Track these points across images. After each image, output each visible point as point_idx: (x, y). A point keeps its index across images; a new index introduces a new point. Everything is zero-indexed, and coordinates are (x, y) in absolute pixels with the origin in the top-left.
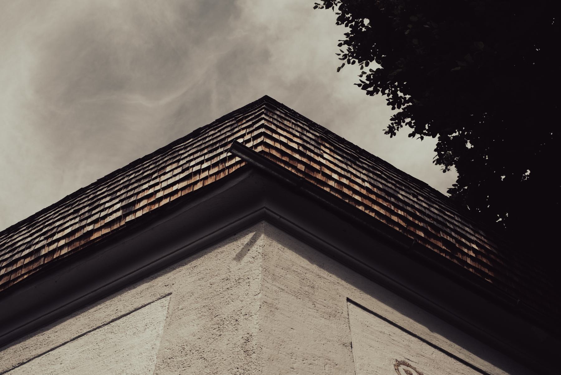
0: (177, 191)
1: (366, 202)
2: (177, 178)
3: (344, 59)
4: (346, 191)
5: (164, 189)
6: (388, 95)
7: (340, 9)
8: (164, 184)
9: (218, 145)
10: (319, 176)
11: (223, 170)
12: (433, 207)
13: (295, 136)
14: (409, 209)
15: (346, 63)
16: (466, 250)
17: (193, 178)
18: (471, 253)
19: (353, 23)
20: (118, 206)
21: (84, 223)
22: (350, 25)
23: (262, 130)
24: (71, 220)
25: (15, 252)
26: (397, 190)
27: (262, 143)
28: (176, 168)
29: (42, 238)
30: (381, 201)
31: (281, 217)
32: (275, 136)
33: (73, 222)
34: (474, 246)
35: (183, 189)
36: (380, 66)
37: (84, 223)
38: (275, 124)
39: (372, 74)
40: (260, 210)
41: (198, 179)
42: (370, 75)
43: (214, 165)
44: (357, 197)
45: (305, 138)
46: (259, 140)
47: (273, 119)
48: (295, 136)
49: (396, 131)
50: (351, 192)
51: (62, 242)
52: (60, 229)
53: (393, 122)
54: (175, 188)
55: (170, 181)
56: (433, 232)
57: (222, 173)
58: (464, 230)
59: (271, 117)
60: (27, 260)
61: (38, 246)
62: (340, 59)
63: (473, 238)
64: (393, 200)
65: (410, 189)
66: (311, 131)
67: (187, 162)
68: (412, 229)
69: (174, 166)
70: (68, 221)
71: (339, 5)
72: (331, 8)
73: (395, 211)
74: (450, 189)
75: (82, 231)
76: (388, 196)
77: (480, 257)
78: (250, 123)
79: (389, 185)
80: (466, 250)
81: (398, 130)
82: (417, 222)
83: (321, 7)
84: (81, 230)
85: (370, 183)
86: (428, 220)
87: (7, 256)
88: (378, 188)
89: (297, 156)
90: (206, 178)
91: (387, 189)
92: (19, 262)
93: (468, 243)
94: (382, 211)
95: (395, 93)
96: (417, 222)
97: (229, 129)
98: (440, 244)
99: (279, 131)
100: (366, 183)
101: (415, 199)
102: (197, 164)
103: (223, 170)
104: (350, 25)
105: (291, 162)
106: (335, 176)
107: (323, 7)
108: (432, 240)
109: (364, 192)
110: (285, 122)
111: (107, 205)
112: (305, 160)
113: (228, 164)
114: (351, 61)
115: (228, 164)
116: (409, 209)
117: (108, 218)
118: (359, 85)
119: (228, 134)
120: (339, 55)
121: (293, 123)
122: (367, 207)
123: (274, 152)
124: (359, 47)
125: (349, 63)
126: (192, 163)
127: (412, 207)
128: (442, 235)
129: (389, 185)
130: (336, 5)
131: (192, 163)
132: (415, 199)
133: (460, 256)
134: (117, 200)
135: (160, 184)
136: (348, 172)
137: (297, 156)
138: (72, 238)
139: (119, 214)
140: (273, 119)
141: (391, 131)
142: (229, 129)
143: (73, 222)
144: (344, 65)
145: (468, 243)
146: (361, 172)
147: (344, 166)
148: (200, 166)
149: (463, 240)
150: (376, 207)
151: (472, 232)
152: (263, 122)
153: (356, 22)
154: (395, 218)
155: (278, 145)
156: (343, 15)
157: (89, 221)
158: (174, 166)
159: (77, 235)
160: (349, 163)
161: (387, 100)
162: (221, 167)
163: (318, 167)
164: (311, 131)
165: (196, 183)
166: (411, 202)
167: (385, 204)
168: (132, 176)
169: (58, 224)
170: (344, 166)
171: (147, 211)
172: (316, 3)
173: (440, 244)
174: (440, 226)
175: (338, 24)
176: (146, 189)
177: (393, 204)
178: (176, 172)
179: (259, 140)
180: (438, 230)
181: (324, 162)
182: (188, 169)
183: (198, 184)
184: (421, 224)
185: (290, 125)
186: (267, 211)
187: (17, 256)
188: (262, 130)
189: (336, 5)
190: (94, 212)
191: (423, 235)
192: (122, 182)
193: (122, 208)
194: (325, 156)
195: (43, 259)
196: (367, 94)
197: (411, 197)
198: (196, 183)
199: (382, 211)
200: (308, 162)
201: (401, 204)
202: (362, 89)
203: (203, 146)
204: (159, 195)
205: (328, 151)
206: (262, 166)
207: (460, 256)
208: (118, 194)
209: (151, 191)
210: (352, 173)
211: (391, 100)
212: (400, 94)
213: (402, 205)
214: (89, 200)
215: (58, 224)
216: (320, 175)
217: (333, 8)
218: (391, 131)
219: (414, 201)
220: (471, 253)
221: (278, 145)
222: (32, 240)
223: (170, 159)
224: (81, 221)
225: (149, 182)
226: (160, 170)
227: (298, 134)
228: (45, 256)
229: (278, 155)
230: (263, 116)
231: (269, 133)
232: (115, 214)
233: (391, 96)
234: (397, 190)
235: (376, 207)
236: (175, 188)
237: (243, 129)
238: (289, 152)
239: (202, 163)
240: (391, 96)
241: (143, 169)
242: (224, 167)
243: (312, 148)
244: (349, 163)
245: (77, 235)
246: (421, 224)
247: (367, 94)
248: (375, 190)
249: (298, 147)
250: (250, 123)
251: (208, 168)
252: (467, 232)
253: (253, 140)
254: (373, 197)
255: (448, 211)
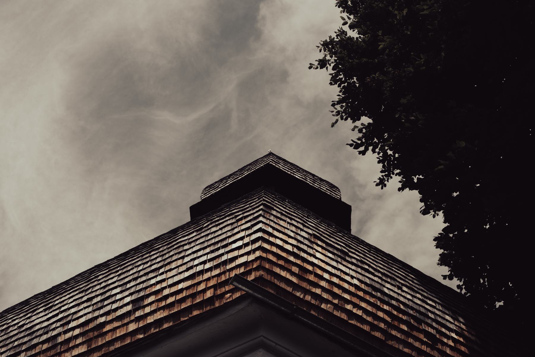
0: (181, 291)
1: (355, 300)
2: (182, 277)
3: (337, 115)
4: (336, 290)
5: (170, 286)
6: (379, 153)
7: (333, 69)
8: (170, 282)
9: (219, 245)
10: (312, 278)
11: (224, 273)
12: (416, 297)
13: (290, 237)
14: (394, 302)
15: (340, 119)
16: (445, 340)
17: (197, 278)
18: (451, 343)
19: (346, 84)
20: (128, 299)
21: (96, 314)
22: (342, 85)
23: (259, 234)
24: (85, 308)
25: (33, 336)
26: (383, 283)
27: (260, 248)
28: (181, 265)
29: (59, 324)
30: (368, 297)
31: (276, 344)
32: (272, 239)
33: (87, 311)
34: (454, 335)
35: (187, 288)
36: (371, 121)
37: (96, 314)
38: (271, 227)
39: (364, 128)
40: (258, 337)
41: (201, 279)
42: (362, 129)
43: (216, 267)
44: (347, 296)
45: (299, 238)
46: (257, 245)
47: (270, 220)
48: (290, 237)
49: (386, 182)
50: (341, 291)
51: (77, 332)
52: (75, 316)
53: (384, 174)
54: (180, 286)
55: (176, 279)
56: (416, 324)
57: (223, 275)
58: (444, 319)
59: (268, 219)
60: (45, 346)
61: (55, 333)
62: (333, 115)
63: (451, 326)
64: (379, 294)
65: (395, 280)
66: (305, 229)
67: (192, 260)
68: (396, 323)
69: (180, 262)
70: (82, 310)
71: (332, 65)
72: (325, 69)
73: (381, 306)
74: (436, 237)
75: (95, 321)
76: (375, 291)
77: (458, 346)
78: (249, 225)
79: (376, 279)
80: (445, 340)
81: (388, 181)
82: (401, 316)
83: (315, 67)
84: (94, 321)
85: (359, 280)
86: (411, 312)
87: (26, 339)
88: (366, 284)
89: (292, 259)
90: (208, 279)
91: (374, 284)
92: (37, 347)
93: (447, 333)
94: (369, 308)
95: (385, 153)
96: (401, 316)
97: (229, 228)
98: (422, 336)
99: (276, 233)
100: (354, 279)
101: (399, 292)
102: (201, 264)
103: (224, 273)
104: (342, 85)
105: (286, 265)
106: (326, 276)
107: (317, 68)
108: (415, 333)
109: (353, 289)
110: (282, 223)
111: (119, 297)
112: (299, 262)
113: (229, 267)
114: (344, 117)
115: (229, 267)
116: (394, 302)
117: (119, 310)
118: (351, 145)
119: (229, 234)
120: (333, 112)
121: (288, 223)
122: (355, 305)
123: (271, 257)
124: (351, 105)
125: (342, 119)
126: (196, 262)
127: (397, 300)
128: (424, 328)
129: (376, 279)
130: (330, 65)
131: (196, 262)
132: (399, 292)
133: (440, 347)
134: (127, 293)
135: (167, 281)
136: (338, 269)
137: (292, 259)
138: (87, 328)
139: (129, 308)
140: (270, 220)
141: (382, 183)
142: (229, 228)
143: (87, 311)
144: (337, 121)
145: (447, 333)
146: (350, 269)
147: (334, 264)
148: (203, 265)
149: (443, 330)
150: (363, 305)
151: (452, 321)
152: (260, 225)
153: (348, 83)
154: (380, 314)
155: (274, 249)
156: (337, 74)
157: (102, 311)
158: (180, 262)
159: (91, 326)
160: (339, 260)
161: (378, 158)
162: (222, 269)
163: (310, 268)
164: (305, 229)
165: (199, 283)
166: (395, 295)
167: (372, 300)
168: (141, 268)
169: (73, 310)
170: (334, 264)
171: (155, 308)
172: (310, 64)
173: (422, 336)
174: (422, 317)
175: (331, 84)
176: (154, 284)
177: (379, 299)
178: (182, 269)
179: (257, 245)
180: (420, 322)
181: (316, 261)
182: (191, 268)
183: (202, 285)
184: (405, 318)
185: (285, 225)
186: (264, 339)
187: (35, 341)
188: (259, 234)
189: (330, 65)
190: (106, 303)
191: (406, 329)
192: (131, 272)
193: (132, 302)
194: (318, 255)
195: (59, 346)
196: (359, 154)
197: (396, 290)
198: (199, 283)
199: (369, 308)
200: (302, 264)
201: (386, 299)
202: (354, 148)
203: (206, 244)
204: (166, 292)
205: (319, 249)
206: (260, 296)
207: (440, 347)
208: (128, 286)
209: (158, 287)
210: (342, 271)
211: (381, 158)
212: (390, 152)
213: (386, 299)
214: (101, 288)
215: (73, 310)
216: (313, 276)
217: (327, 68)
218: (382, 183)
219: (398, 294)
220: (451, 343)
221: (274, 249)
222: (49, 325)
223: (176, 254)
224: (94, 311)
225: (156, 276)
226: (166, 265)
227: (292, 234)
228: (62, 343)
229: (274, 259)
230: (261, 219)
231: (266, 237)
232: (125, 308)
233: (381, 154)
234: (383, 283)
235: (363, 305)
236: (180, 286)
237: (243, 230)
238: (284, 255)
239: (204, 263)
240: (381, 154)
241: (151, 260)
242: (225, 269)
243: (305, 248)
244: (339, 260)
245: (91, 326)
246: (405, 318)
247: (359, 154)
248: (363, 286)
249: (293, 249)
250: (249, 225)
251: (210, 269)
252: (447, 320)
253: (252, 244)
254: (361, 294)
255: (430, 300)
